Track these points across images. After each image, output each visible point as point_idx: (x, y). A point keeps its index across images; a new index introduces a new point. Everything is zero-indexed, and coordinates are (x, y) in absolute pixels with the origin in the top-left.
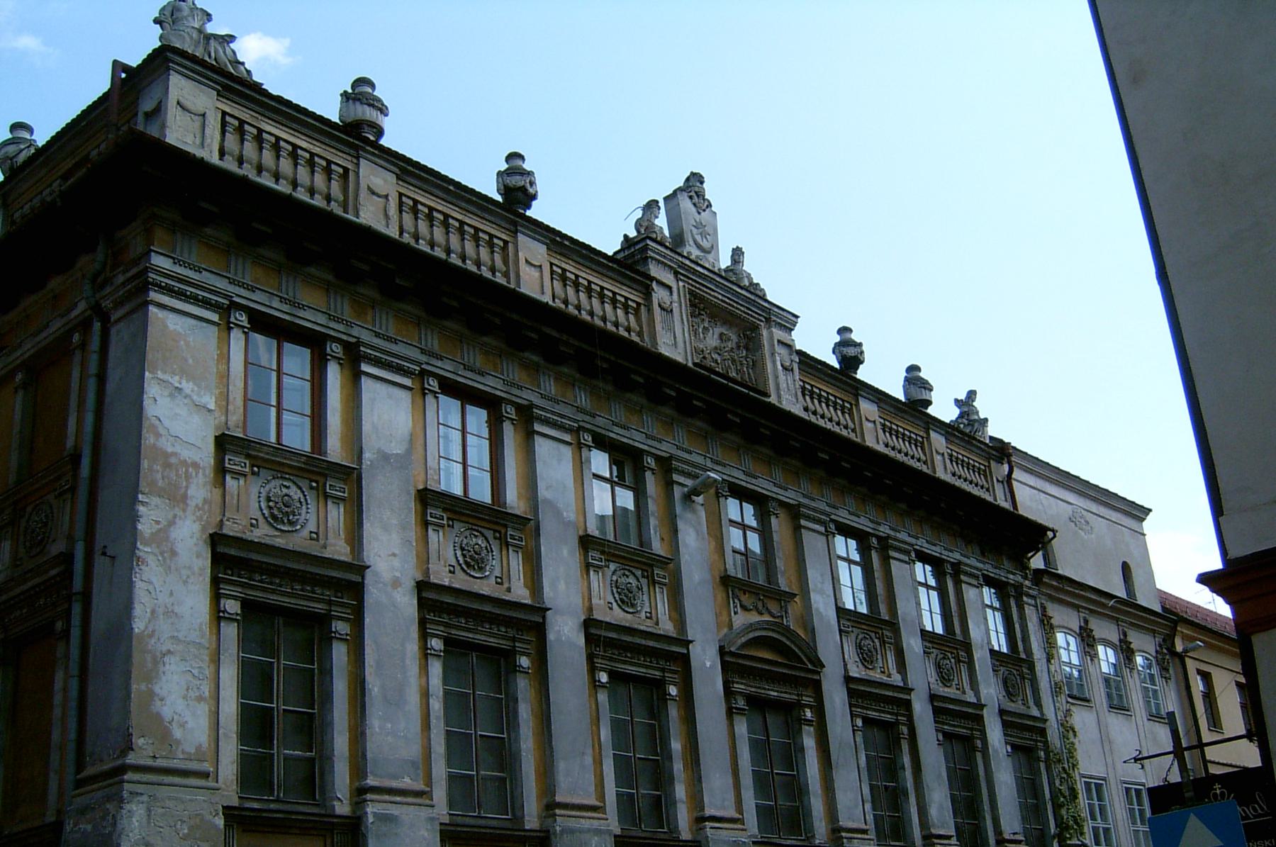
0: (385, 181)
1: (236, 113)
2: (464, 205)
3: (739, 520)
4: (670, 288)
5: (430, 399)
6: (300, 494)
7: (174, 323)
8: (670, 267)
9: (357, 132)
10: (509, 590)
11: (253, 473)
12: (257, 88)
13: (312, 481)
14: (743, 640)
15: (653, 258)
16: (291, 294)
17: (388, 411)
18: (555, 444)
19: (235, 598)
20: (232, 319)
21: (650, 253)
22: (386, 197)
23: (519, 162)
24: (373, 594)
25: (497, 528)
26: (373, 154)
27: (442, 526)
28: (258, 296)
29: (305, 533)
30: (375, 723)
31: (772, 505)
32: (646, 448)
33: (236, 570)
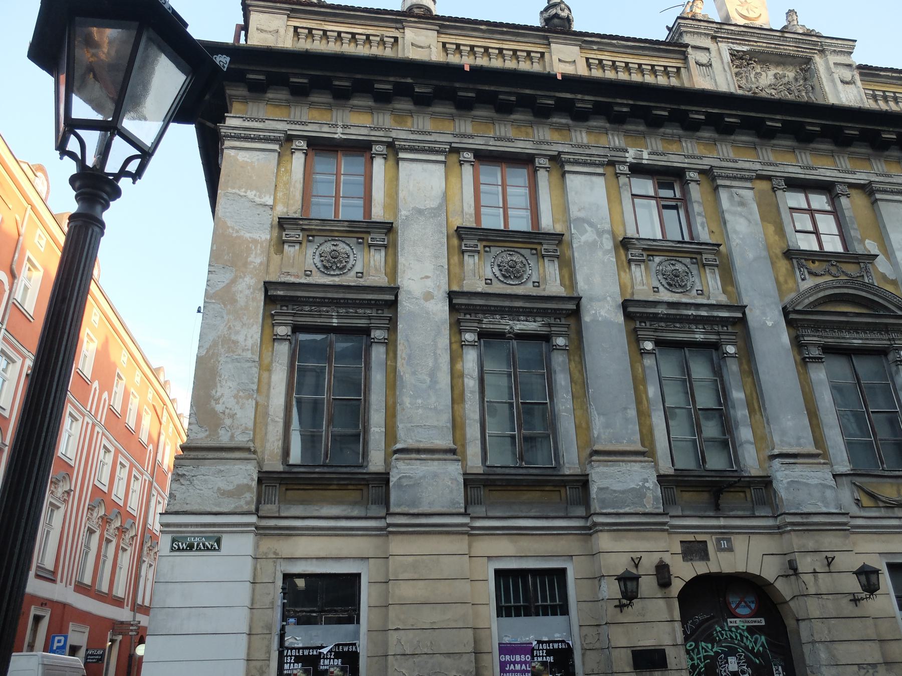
3: (806, 207)
4: (708, 49)
5: (623, 180)
7: (242, 156)
8: (708, 34)
10: (544, 290)
13: (358, 238)
14: (812, 299)
15: (687, 32)
16: (766, 158)
17: (588, 193)
19: (285, 324)
20: (537, 164)
21: (683, 29)
24: (405, 305)
25: (694, 256)
26: (415, 22)
27: (643, 261)
28: (310, 127)
29: (353, 273)
31: (839, 189)
32: (686, 165)
33: (290, 307)
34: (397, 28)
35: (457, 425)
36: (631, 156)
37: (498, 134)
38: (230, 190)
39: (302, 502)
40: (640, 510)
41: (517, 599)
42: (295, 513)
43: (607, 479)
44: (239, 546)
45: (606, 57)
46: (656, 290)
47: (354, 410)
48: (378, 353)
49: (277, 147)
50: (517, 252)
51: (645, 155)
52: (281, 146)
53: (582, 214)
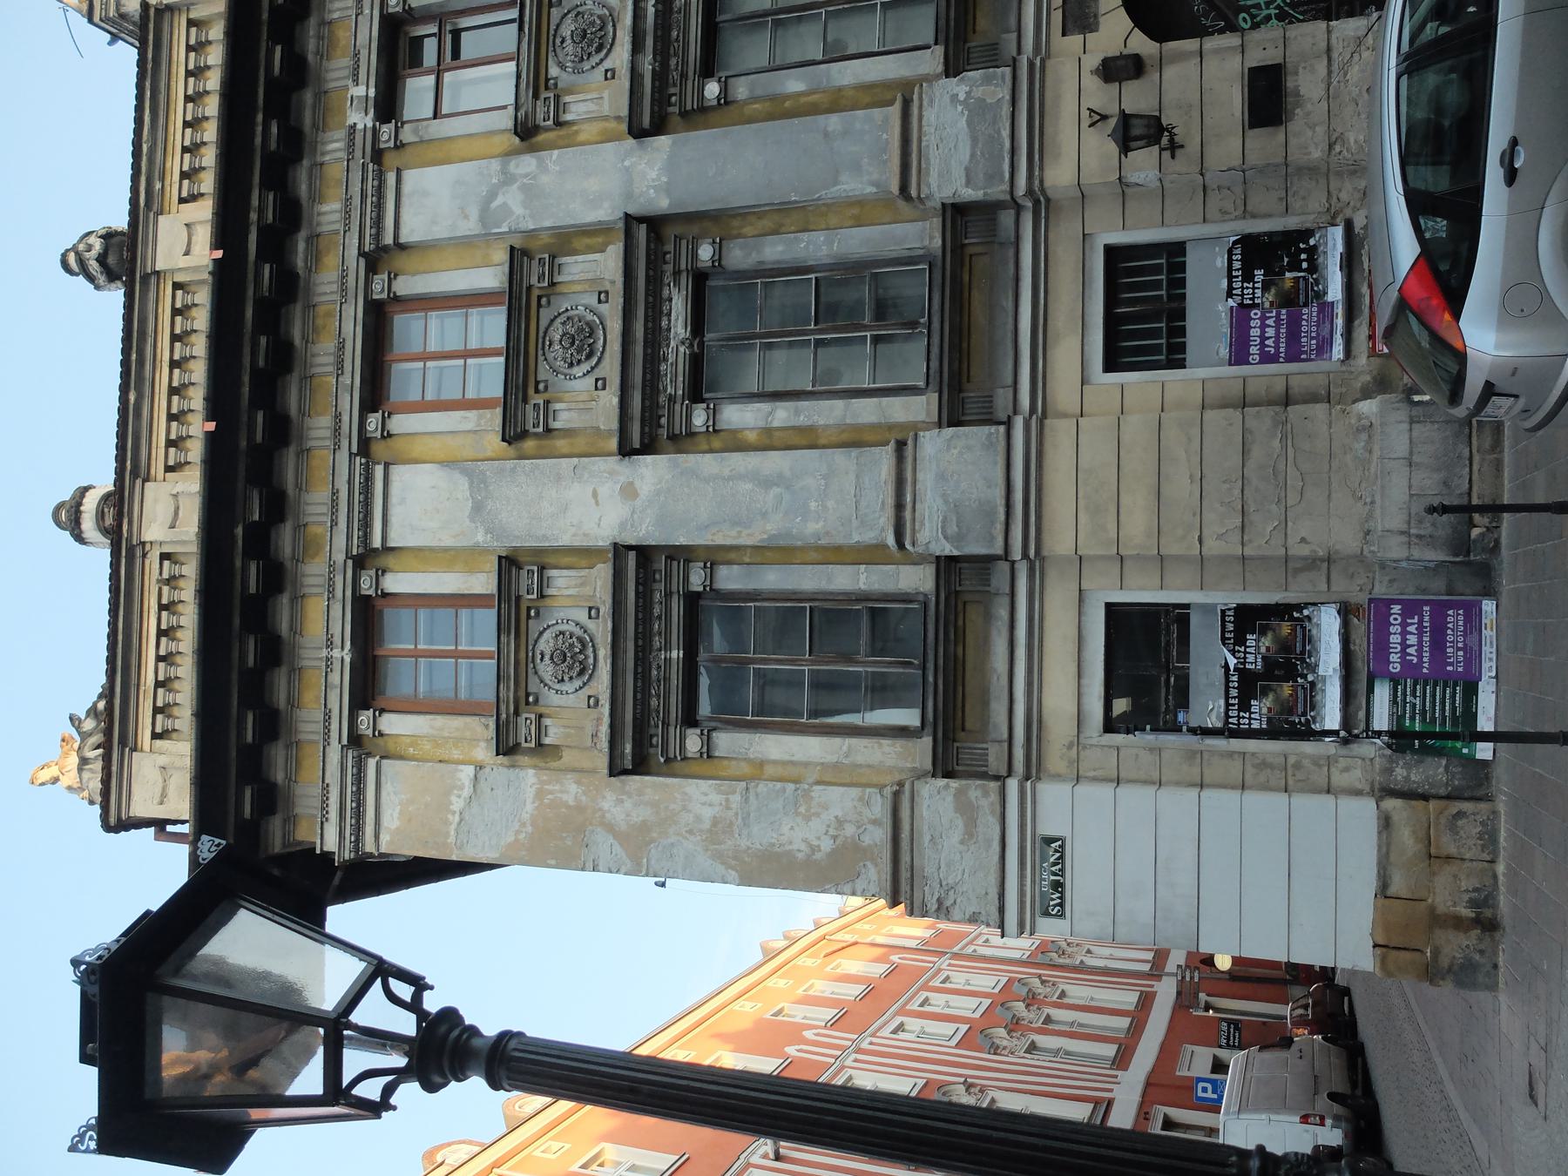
0: (156, 501)
1: (149, 721)
2: (148, 367)
5: (407, 135)
6: (547, 635)
7: (391, 820)
9: (119, 259)
11: (536, 701)
12: (108, 693)
15: (118, 9)
17: (433, 201)
18: (405, 200)
20: (384, 296)
22: (175, 496)
23: (90, 504)
24: (646, 532)
28: (334, 704)
29: (591, 625)
30: (812, 529)
33: (652, 731)
34: (144, 555)
35: (855, 439)
36: (361, 119)
37: (330, 369)
38: (451, 839)
39: (985, 703)
40: (1006, 110)
41: (1155, 334)
42: (1002, 714)
43: (951, 173)
44: (1056, 806)
45: (176, 164)
46: (610, 75)
47: (829, 618)
48: (730, 579)
49: (371, 763)
50: (545, 333)
51: (360, 91)
52: (369, 755)
53: (474, 213)
